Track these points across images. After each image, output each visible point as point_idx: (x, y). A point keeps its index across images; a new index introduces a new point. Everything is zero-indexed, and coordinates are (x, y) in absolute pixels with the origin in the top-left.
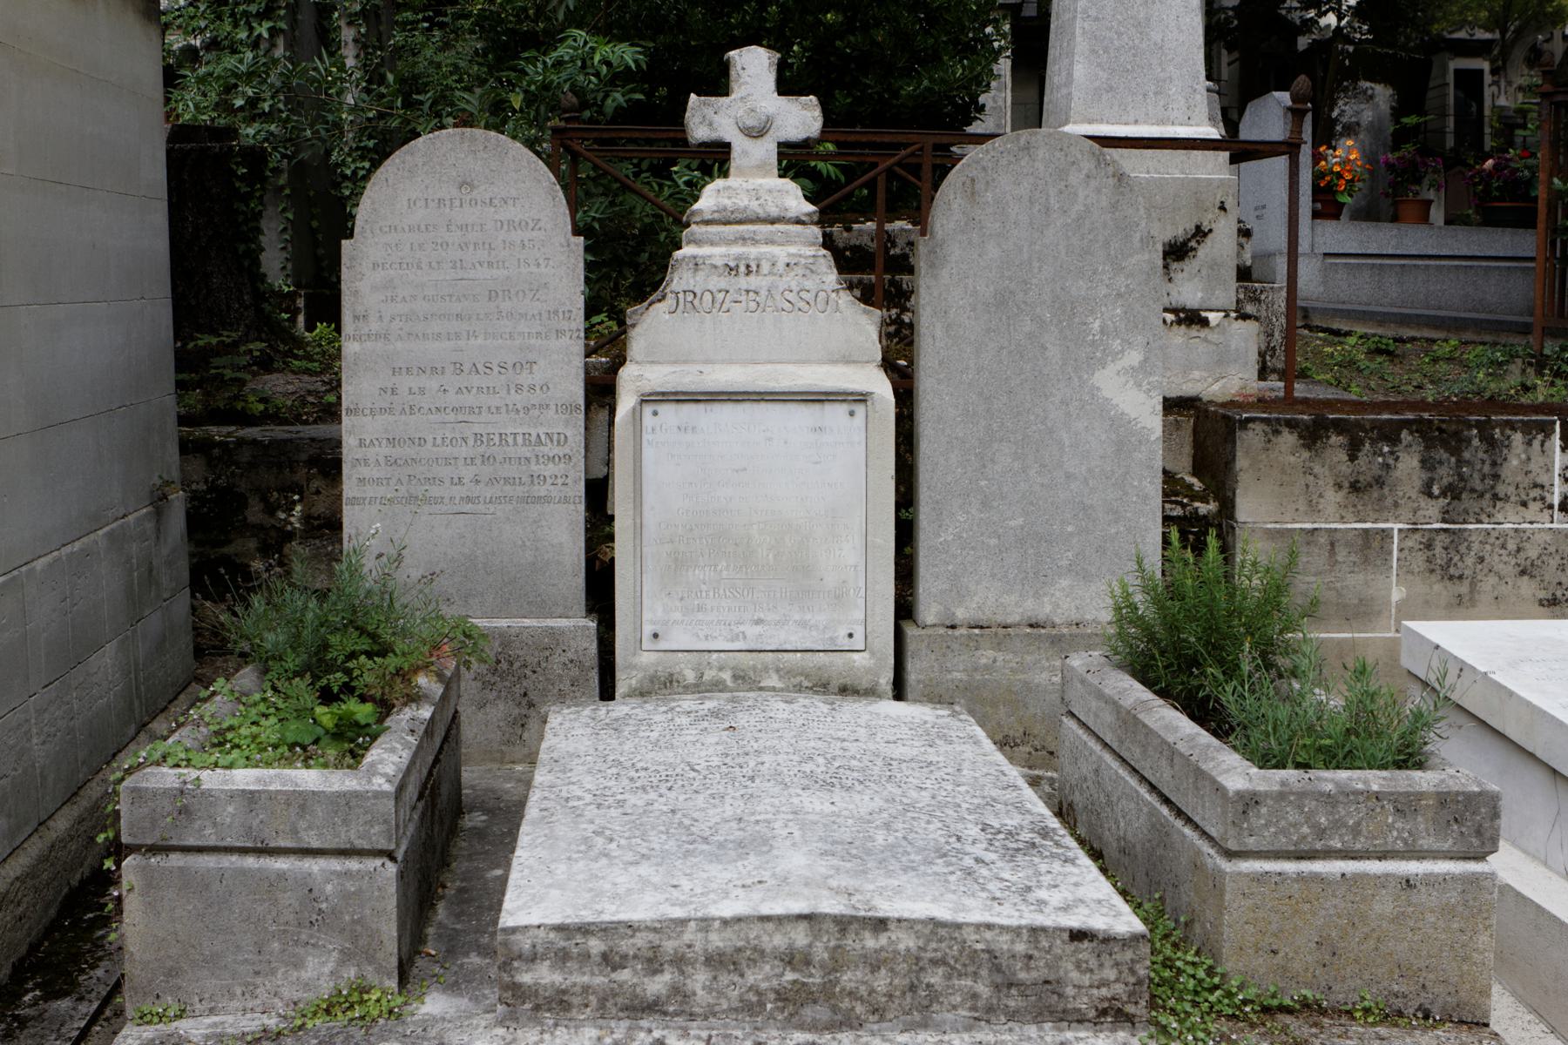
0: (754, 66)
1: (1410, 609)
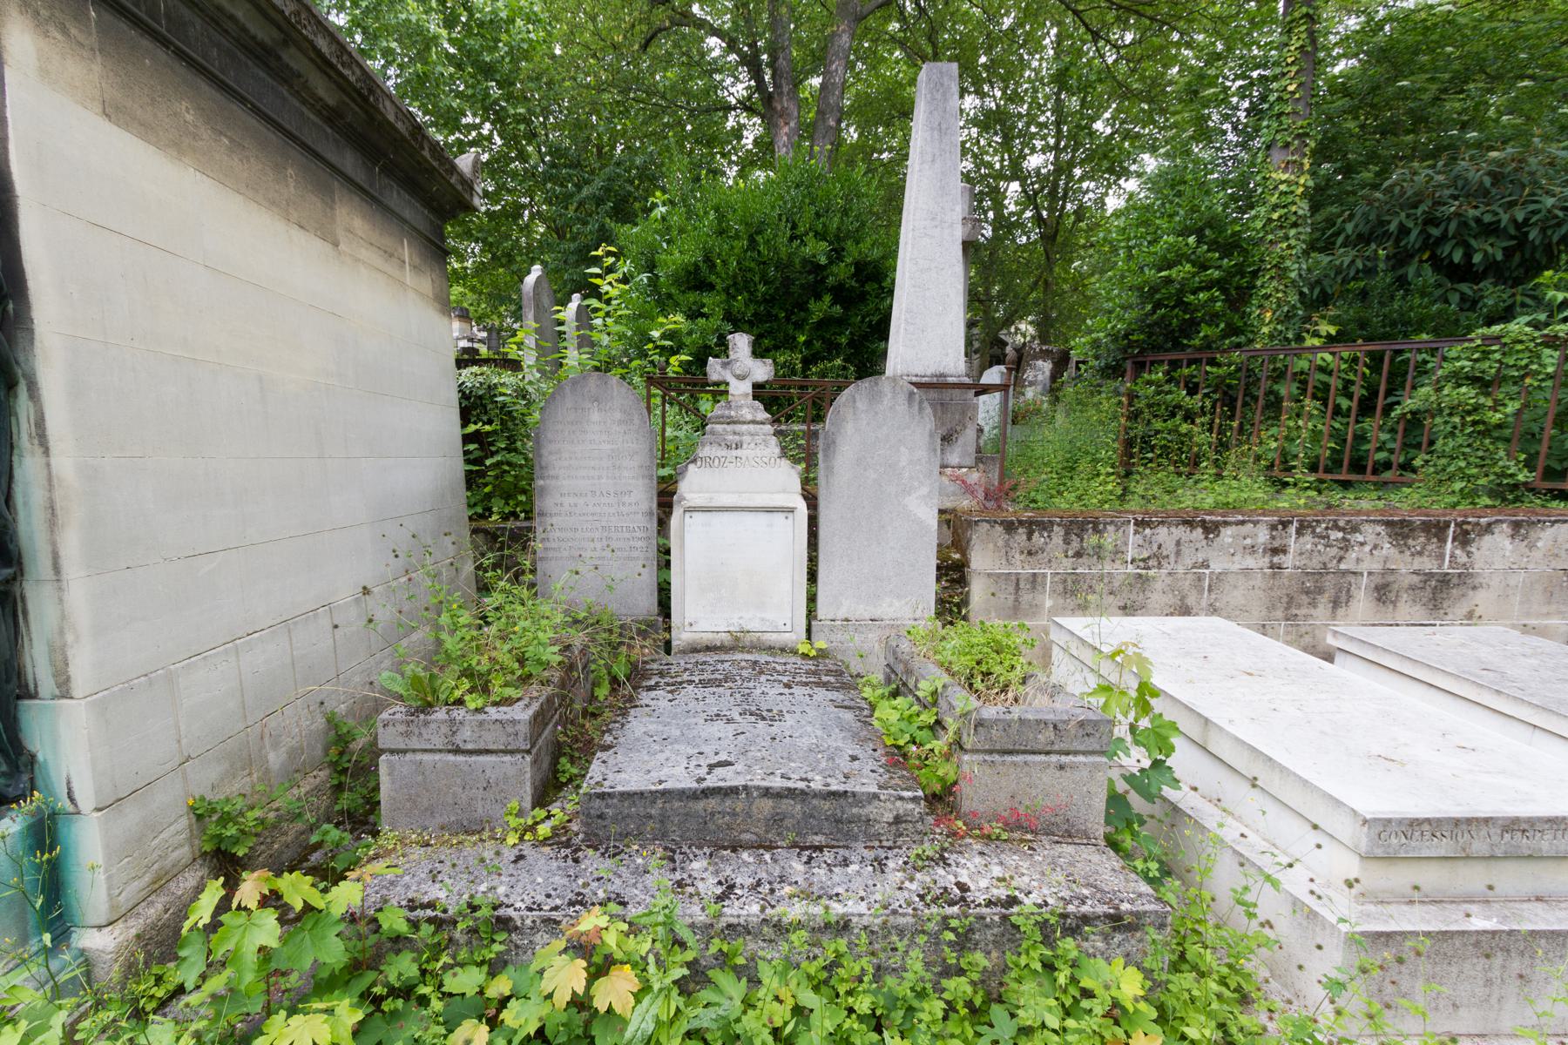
0: (741, 343)
1: (1055, 611)
